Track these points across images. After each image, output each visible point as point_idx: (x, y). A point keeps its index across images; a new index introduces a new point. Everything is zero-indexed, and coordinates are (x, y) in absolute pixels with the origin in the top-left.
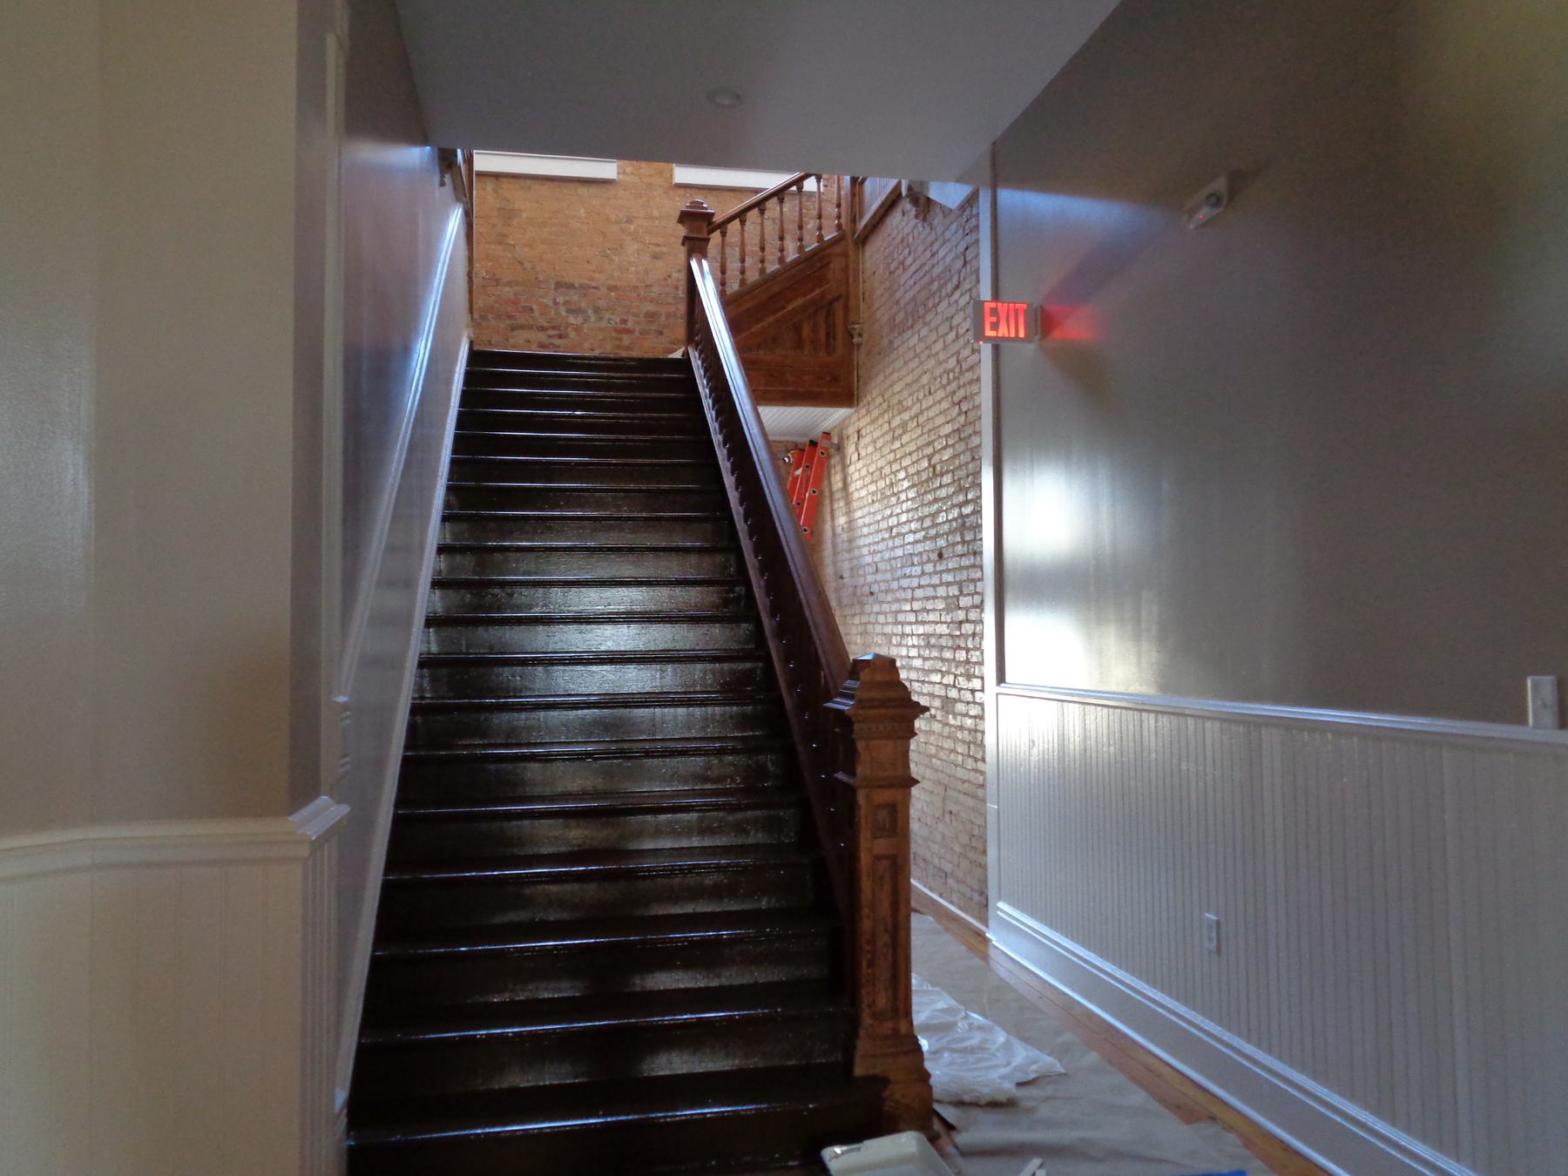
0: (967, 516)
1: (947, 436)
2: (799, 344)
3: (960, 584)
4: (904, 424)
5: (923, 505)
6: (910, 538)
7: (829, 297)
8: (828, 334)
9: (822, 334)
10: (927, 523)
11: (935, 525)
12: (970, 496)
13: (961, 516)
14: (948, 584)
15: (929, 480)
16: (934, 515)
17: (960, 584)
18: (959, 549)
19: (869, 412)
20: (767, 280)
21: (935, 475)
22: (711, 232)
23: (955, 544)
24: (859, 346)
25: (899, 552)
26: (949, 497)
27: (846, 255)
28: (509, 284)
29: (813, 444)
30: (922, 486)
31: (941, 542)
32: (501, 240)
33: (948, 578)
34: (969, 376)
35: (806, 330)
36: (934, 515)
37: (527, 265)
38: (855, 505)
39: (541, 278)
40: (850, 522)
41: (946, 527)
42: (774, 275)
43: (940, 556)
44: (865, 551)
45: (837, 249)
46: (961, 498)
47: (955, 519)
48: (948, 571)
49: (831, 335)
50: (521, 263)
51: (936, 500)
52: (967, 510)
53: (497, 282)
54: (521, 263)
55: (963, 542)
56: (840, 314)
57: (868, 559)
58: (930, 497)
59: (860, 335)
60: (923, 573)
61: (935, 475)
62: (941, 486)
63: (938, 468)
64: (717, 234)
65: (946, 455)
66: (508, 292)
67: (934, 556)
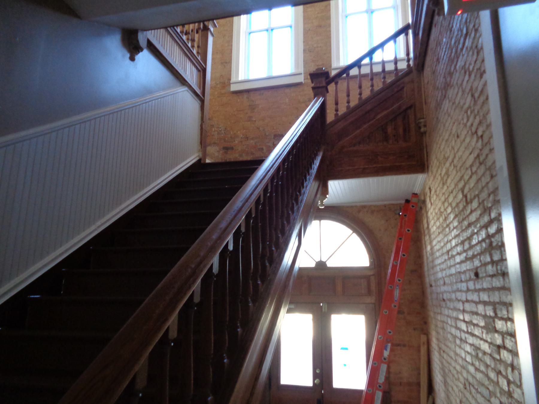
0: (493, 235)
1: (471, 166)
2: (386, 138)
3: (494, 305)
4: (448, 170)
5: (463, 231)
6: (458, 259)
7: (404, 107)
8: (405, 130)
9: (401, 131)
10: (467, 246)
11: (471, 247)
12: (493, 215)
13: (489, 236)
14: (485, 303)
15: (465, 208)
16: (470, 238)
17: (494, 305)
18: (490, 269)
19: (432, 172)
20: (362, 103)
21: (467, 203)
22: (329, 83)
23: (485, 264)
24: (425, 132)
25: (453, 271)
26: (478, 220)
27: (413, 81)
28: (253, 139)
29: (407, 201)
30: (461, 216)
31: (477, 263)
32: (250, 119)
33: (484, 297)
34: (482, 99)
35: (390, 130)
36: (470, 238)
37: (261, 129)
38: (433, 236)
39: (267, 134)
40: (432, 248)
41: (478, 248)
42: (368, 100)
43: (477, 275)
44: (438, 268)
45: (407, 79)
46: (486, 219)
47: (483, 240)
48: (483, 290)
49: (406, 130)
50: (258, 128)
51: (469, 225)
52: (492, 230)
53: (247, 138)
54: (258, 128)
55: (493, 262)
56: (412, 117)
57: (440, 275)
58: (466, 223)
59: (425, 126)
60: (468, 290)
61: (467, 203)
62: (472, 212)
63: (469, 197)
64: (333, 84)
65: (472, 183)
66: (252, 142)
67: (473, 276)
